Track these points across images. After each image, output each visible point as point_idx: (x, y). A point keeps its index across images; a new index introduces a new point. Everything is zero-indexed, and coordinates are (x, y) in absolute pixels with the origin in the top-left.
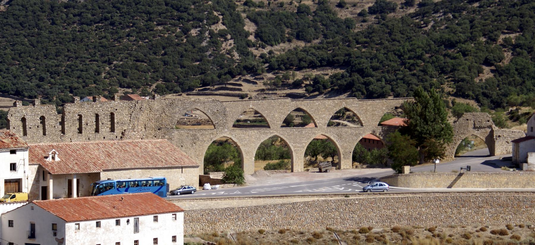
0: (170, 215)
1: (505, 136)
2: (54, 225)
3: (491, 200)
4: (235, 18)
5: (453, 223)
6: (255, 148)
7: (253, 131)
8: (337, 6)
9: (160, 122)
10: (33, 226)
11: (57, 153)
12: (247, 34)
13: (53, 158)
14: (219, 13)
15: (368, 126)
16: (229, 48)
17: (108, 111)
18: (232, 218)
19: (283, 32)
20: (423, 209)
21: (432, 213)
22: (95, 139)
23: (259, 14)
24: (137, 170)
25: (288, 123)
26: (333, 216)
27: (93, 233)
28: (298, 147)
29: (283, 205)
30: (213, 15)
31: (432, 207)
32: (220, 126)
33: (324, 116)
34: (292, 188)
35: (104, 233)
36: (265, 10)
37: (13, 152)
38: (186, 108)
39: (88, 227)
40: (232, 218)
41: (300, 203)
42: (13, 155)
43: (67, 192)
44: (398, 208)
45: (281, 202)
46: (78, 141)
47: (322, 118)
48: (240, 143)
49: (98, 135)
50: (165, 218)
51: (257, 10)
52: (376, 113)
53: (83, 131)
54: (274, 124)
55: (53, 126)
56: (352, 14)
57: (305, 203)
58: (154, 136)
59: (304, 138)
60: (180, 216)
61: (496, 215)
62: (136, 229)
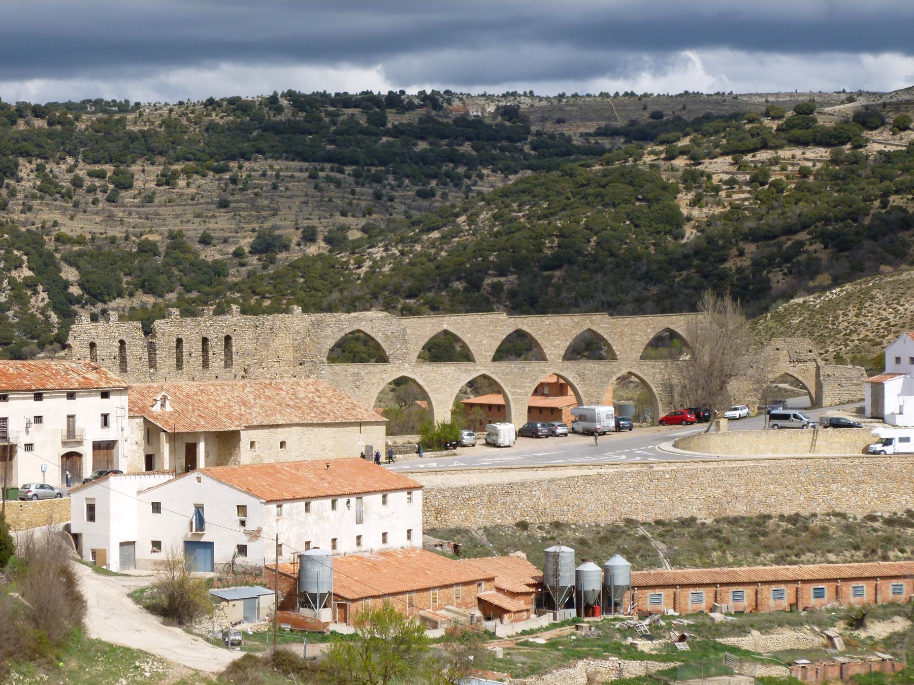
1: (837, 375)
3: (877, 470)
4: (47, 260)
5: (818, 509)
6: (451, 395)
7: (447, 368)
8: (201, 242)
9: (302, 352)
11: (169, 398)
12: (67, 284)
14: (21, 252)
15: (624, 359)
16: (41, 305)
17: (223, 332)
18: (473, 502)
19: (119, 281)
20: (772, 487)
21: (785, 493)
22: (201, 379)
23: (80, 254)
24: (294, 429)
25: (501, 355)
26: (630, 498)
28: (519, 394)
29: (551, 481)
30: (13, 253)
31: (786, 482)
32: (397, 358)
33: (557, 342)
34: (536, 456)
36: (89, 247)
38: (343, 329)
40: (473, 502)
41: (578, 477)
43: (184, 464)
44: (732, 485)
45: (548, 477)
46: (186, 385)
47: (555, 347)
48: (429, 387)
49: (207, 374)
52: (637, 338)
53: (184, 366)
54: (480, 354)
55: (138, 357)
56: (222, 254)
57: (586, 478)
58: (292, 375)
59: (527, 379)
60: (417, 495)
61: (885, 495)
62: (359, 521)
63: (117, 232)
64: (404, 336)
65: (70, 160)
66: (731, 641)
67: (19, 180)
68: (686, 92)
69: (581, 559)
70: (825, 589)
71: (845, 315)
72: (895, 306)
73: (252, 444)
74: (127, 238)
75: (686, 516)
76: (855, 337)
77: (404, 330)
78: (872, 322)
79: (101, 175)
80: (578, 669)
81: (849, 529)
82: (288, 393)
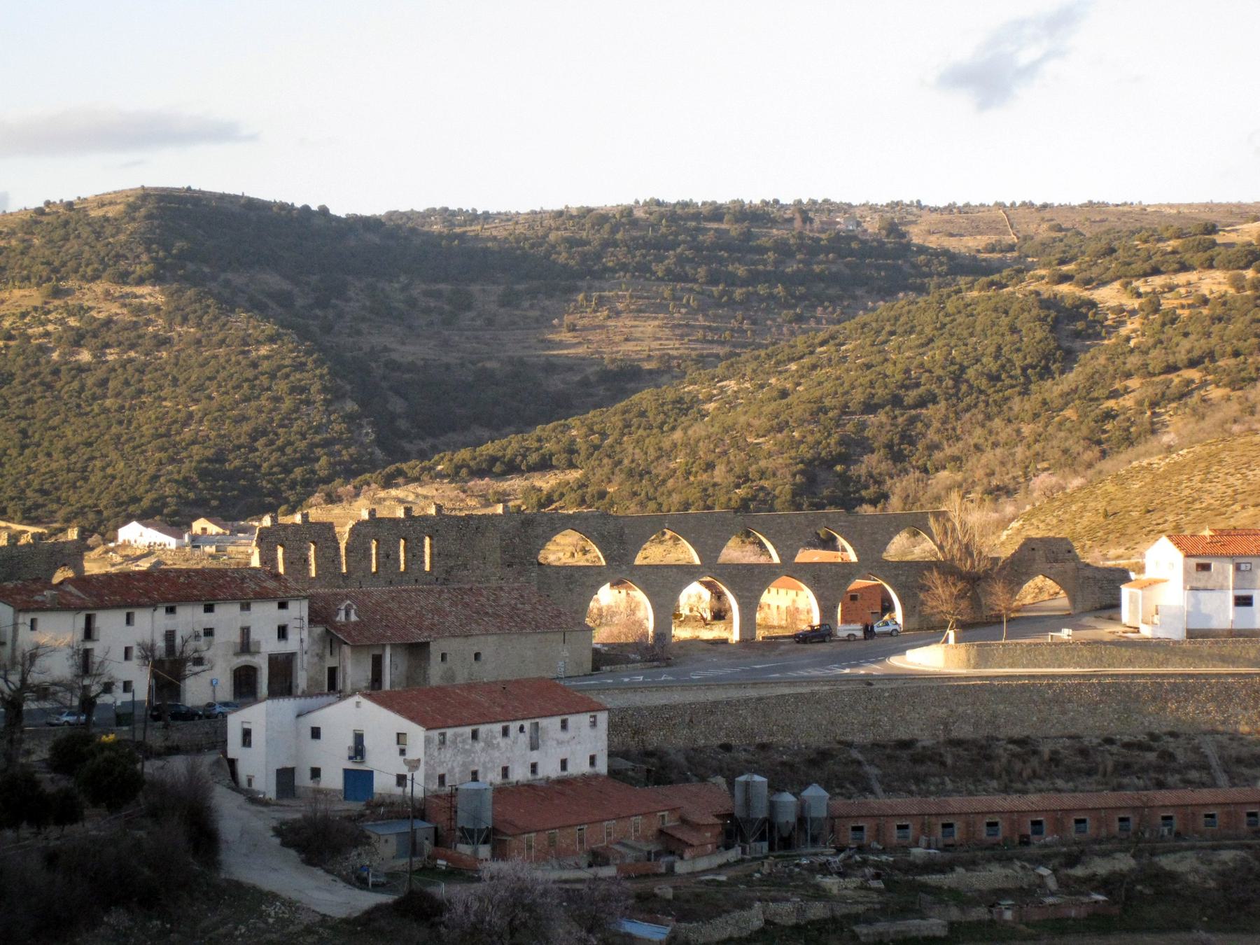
0: (585, 718)
2: (401, 737)
10: (359, 738)
13: (347, 614)
20: (1002, 707)
27: (466, 750)
29: (760, 699)
35: (483, 750)
37: (283, 605)
39: (458, 739)
42: (283, 612)
50: (579, 721)
51: (407, 376)
57: (797, 697)
63: (451, 358)
64: (621, 536)
65: (403, 279)
66: (933, 879)
67: (348, 300)
68: (1090, 202)
69: (775, 787)
70: (1045, 824)
71: (1190, 480)
72: (1244, 471)
73: (444, 657)
74: (462, 365)
75: (905, 737)
76: (1197, 505)
77: (622, 528)
78: (1218, 488)
79: (438, 295)
80: (753, 912)
81: (1084, 752)
82: (488, 600)
